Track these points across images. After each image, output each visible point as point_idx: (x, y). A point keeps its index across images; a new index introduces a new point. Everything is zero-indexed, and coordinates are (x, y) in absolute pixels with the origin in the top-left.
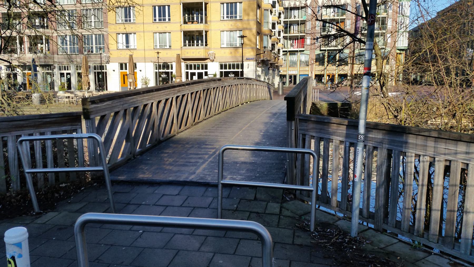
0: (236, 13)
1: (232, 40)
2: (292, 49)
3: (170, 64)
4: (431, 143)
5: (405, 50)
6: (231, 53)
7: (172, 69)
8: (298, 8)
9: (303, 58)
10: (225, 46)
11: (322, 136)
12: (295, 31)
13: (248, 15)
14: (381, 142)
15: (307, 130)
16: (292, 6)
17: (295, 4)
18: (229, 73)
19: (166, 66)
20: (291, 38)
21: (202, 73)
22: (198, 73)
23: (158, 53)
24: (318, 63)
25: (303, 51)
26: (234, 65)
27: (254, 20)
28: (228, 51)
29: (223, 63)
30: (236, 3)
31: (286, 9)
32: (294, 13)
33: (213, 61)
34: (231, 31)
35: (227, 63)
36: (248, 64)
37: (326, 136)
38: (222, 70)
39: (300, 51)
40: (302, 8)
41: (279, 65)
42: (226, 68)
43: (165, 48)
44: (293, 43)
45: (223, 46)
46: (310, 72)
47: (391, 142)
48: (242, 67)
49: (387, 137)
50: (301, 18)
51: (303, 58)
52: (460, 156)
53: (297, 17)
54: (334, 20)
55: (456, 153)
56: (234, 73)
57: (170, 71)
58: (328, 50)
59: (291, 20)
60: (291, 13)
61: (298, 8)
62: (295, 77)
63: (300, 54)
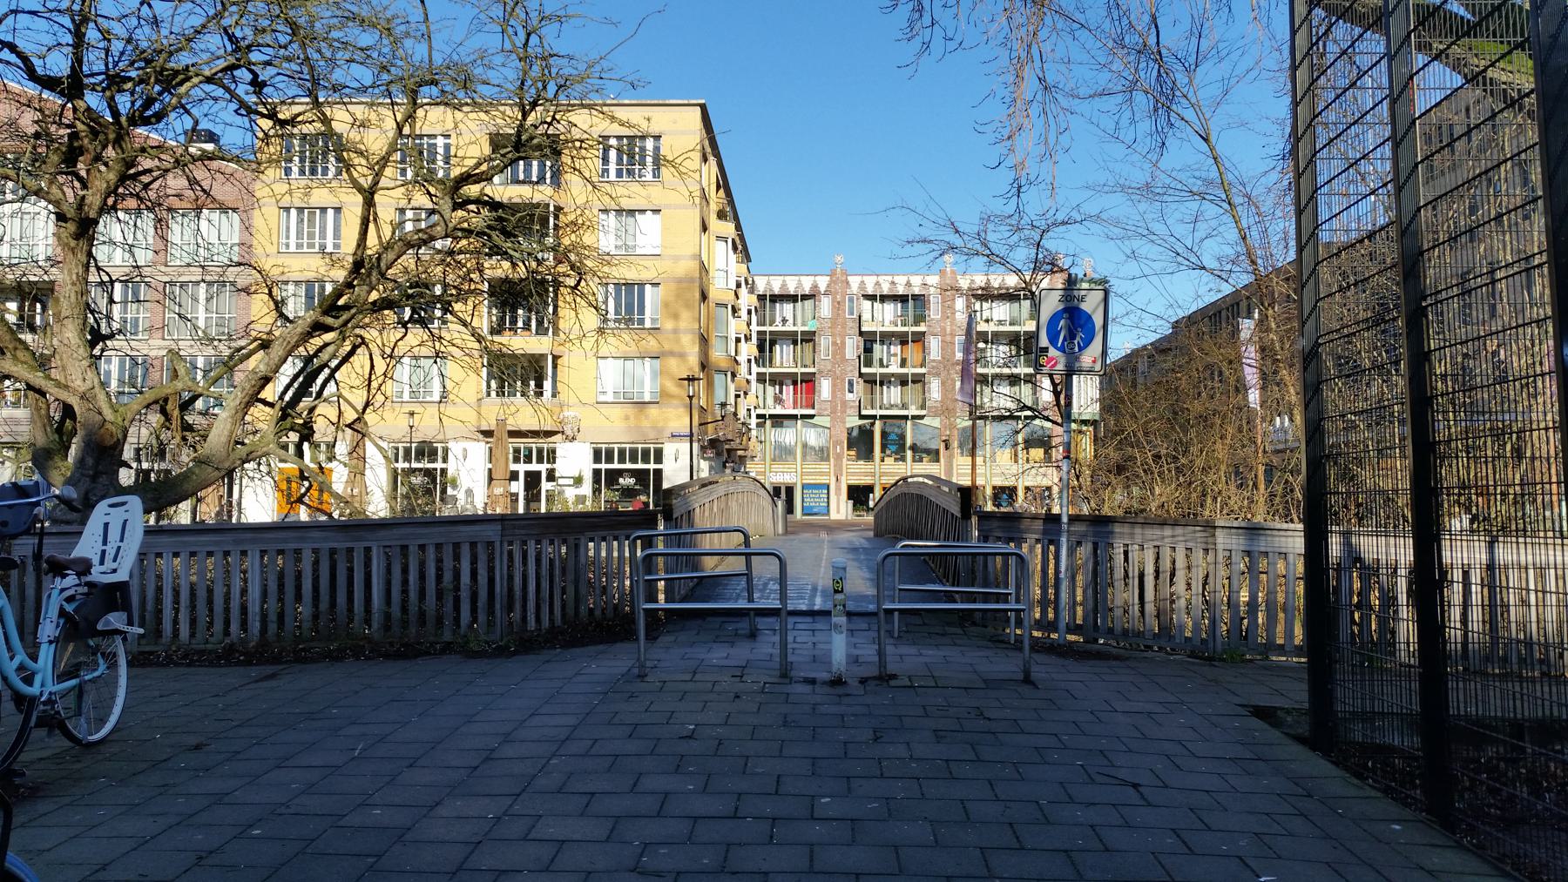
0: (642, 311)
1: (628, 382)
2: (779, 411)
3: (439, 445)
4: (1138, 530)
5: (1094, 423)
6: (627, 418)
7: (445, 460)
8: (793, 298)
9: (813, 437)
10: (610, 397)
11: (1011, 535)
12: (785, 359)
13: (676, 317)
14: (1085, 536)
15: (991, 530)
16: (777, 291)
17: (784, 285)
18: (620, 473)
19: (427, 450)
20: (777, 380)
21: (539, 473)
22: (528, 474)
23: (412, 414)
24: (853, 453)
25: (812, 417)
26: (634, 453)
27: (692, 331)
28: (617, 412)
29: (604, 446)
30: (642, 285)
31: (761, 298)
32: (781, 310)
33: (574, 439)
34: (626, 358)
35: (616, 446)
36: (465, 450)
37: (1016, 535)
38: (598, 466)
39: (804, 417)
40: (805, 297)
41: (749, 453)
42: (610, 459)
43: (428, 399)
44: (781, 392)
45: (602, 398)
46: (833, 479)
47: (1096, 534)
48: (659, 459)
49: (1091, 529)
50: (803, 325)
51: (813, 437)
52: (1166, 540)
53: (791, 321)
54: (893, 334)
55: (1163, 538)
56: (633, 473)
57: (439, 465)
58: (882, 417)
59: (773, 328)
60: (773, 309)
61: (793, 298)
62: (790, 490)
63: (803, 426)
